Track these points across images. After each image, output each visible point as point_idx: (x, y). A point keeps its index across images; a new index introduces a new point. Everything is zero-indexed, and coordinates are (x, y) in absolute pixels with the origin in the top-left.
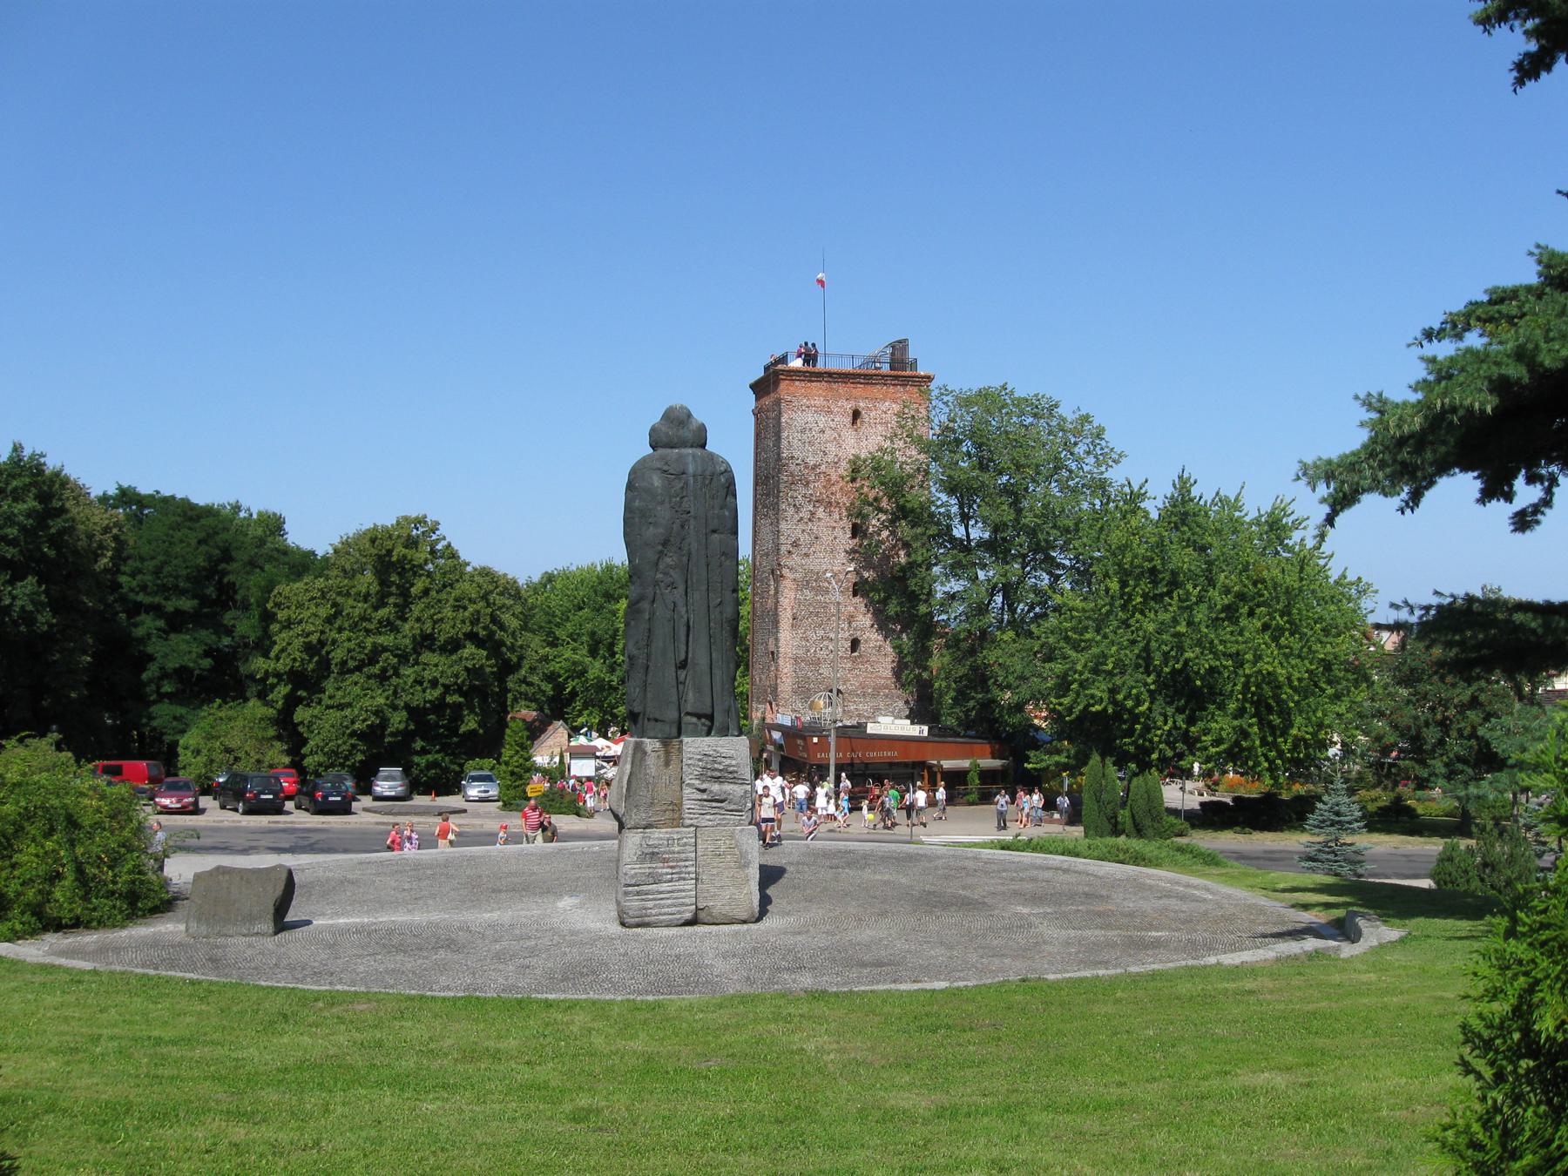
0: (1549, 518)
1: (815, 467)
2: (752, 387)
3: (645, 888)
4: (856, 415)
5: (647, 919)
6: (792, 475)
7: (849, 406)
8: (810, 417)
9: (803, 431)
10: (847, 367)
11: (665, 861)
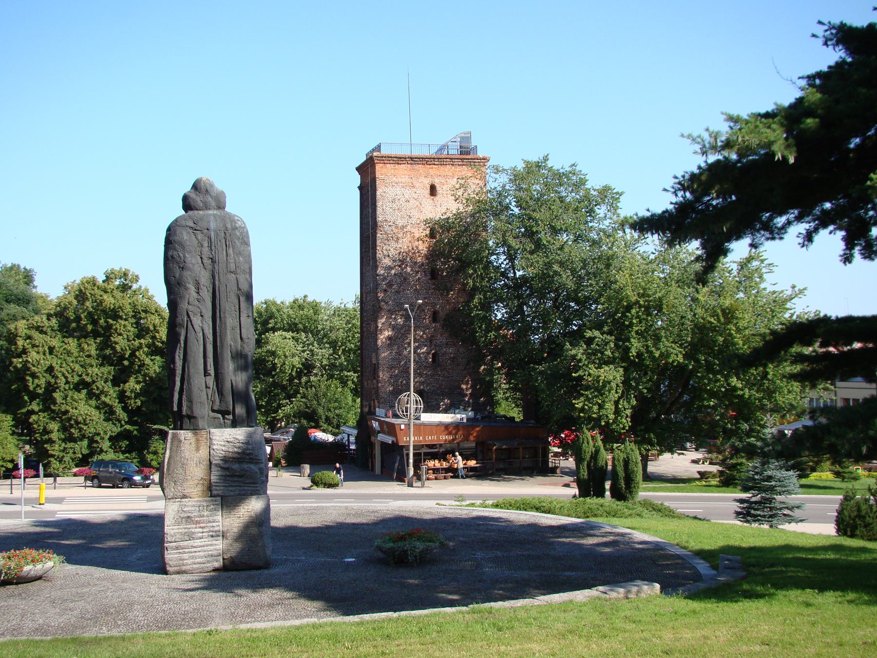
0: (373, 147)
1: (403, 227)
2: (358, 169)
3: (182, 544)
4: (433, 190)
5: (184, 568)
6: (386, 233)
7: (427, 182)
8: (398, 190)
9: (393, 201)
10: (425, 152)
11: (198, 522)
